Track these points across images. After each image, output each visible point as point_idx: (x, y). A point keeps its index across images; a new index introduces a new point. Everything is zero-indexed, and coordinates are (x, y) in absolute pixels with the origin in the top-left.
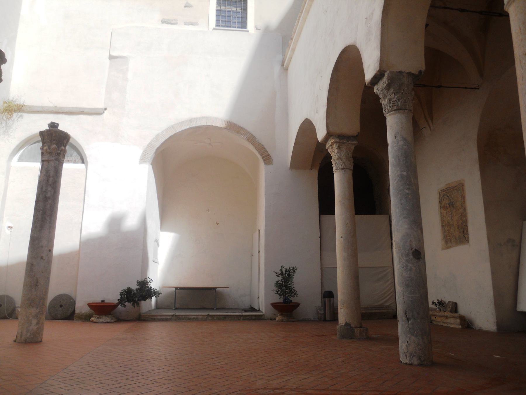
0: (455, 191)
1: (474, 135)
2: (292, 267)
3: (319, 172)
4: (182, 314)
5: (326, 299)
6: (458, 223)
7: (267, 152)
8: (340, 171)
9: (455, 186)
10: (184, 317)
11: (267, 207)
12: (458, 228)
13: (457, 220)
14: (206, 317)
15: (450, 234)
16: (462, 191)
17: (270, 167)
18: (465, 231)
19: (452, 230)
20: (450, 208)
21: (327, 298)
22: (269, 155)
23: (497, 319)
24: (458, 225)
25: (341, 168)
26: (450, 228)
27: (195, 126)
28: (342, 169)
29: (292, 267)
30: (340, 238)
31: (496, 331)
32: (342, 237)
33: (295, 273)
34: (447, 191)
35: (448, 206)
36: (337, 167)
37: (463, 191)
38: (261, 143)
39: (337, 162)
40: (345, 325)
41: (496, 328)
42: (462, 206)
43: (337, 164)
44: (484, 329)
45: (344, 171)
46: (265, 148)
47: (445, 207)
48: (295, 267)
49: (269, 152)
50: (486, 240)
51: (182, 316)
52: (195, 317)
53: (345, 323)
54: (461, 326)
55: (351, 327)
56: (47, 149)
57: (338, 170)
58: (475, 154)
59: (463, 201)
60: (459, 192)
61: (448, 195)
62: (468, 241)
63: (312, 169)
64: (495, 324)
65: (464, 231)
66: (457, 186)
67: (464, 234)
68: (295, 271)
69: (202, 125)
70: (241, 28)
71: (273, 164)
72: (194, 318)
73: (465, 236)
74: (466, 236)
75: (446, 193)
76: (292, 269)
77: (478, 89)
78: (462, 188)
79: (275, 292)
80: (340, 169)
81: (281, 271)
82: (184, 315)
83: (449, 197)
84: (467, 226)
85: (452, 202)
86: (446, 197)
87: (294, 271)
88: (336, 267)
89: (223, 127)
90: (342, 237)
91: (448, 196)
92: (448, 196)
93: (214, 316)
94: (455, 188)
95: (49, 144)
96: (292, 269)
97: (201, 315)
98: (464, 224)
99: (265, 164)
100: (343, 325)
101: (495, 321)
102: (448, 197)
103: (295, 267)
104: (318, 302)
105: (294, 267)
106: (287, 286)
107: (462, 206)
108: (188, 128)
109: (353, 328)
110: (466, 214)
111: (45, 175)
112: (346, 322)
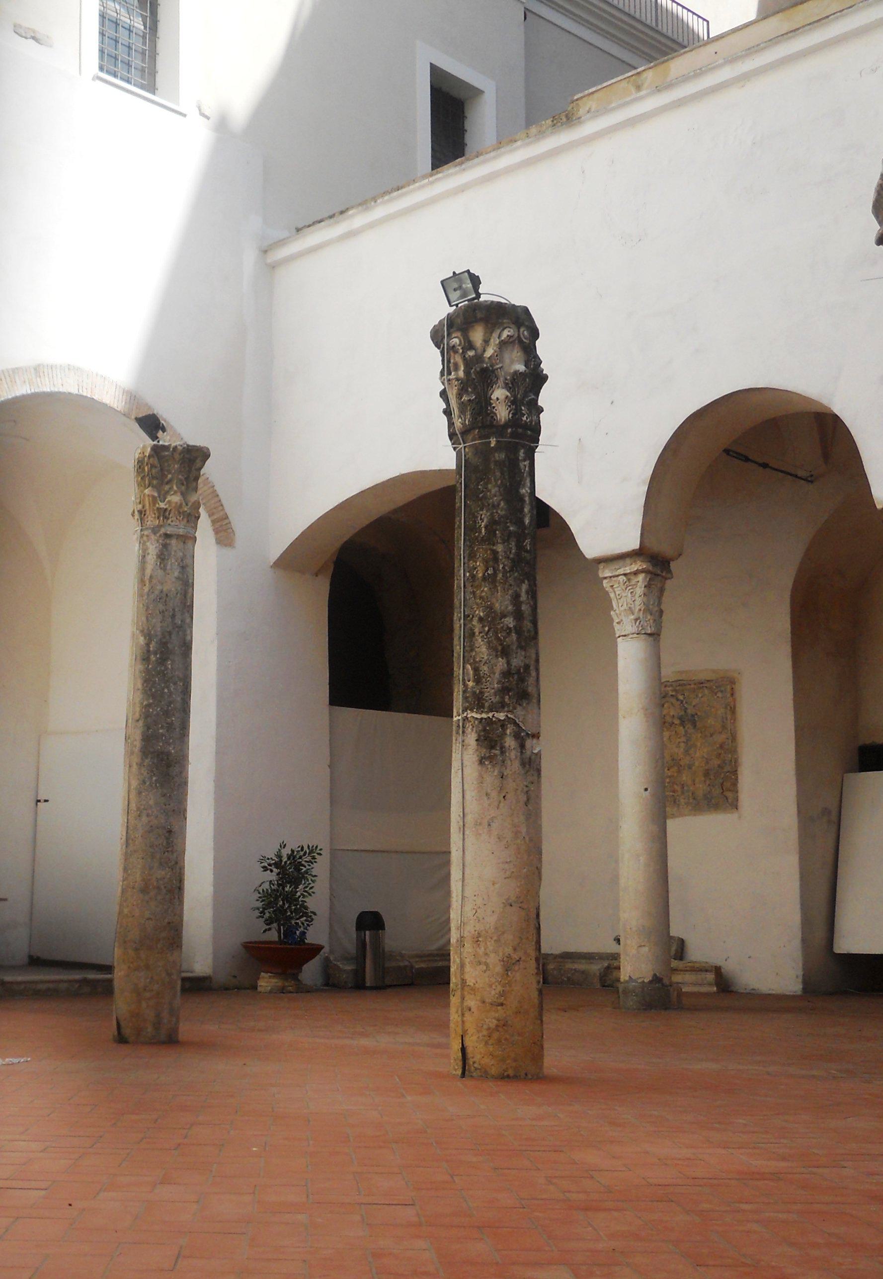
0: (706, 691)
1: (785, 579)
2: (309, 846)
3: (332, 584)
4: (20, 978)
5: (367, 933)
6: (707, 763)
7: (223, 509)
8: (645, 639)
9: (708, 681)
10: (22, 987)
11: (223, 669)
12: (707, 774)
13: (703, 757)
14: (77, 986)
15: (676, 787)
16: (729, 695)
17: (226, 551)
18: (727, 785)
19: (684, 778)
20: (684, 727)
21: (369, 930)
22: (225, 519)
23: (804, 969)
24: (706, 768)
25: (649, 632)
26: (679, 771)
27: (49, 390)
28: (650, 635)
29: (309, 846)
30: (643, 790)
31: (799, 993)
32: (646, 790)
33: (316, 862)
34: (678, 688)
35: (677, 722)
36: (638, 627)
37: (732, 695)
38: (210, 479)
39: (641, 617)
40: (651, 982)
41: (801, 987)
42: (724, 727)
43: (640, 622)
44: (764, 992)
45: (654, 640)
46: (218, 496)
47: (667, 724)
48: (317, 847)
49: (228, 509)
50: (793, 809)
51: (20, 983)
52: (51, 986)
53: (653, 977)
54: (715, 988)
55: (663, 985)
56: (181, 504)
57: (642, 636)
58: (783, 622)
59: (729, 717)
60: (720, 695)
61: (681, 697)
62: (734, 805)
63: (317, 576)
64: (800, 980)
65: (725, 783)
66: (712, 680)
67: (723, 789)
68: (317, 856)
69: (66, 391)
70: (142, 87)
71: (234, 547)
72: (48, 990)
73: (724, 793)
74: (729, 794)
75: (672, 691)
76: (308, 851)
77: (812, 482)
78: (729, 687)
79: (257, 913)
80: (645, 634)
81: (279, 856)
82: (24, 982)
83: (682, 702)
84: (735, 772)
85: (693, 716)
86: (673, 700)
87: (314, 858)
88: (444, 849)
89: (119, 410)
90: (646, 790)
91: (678, 700)
92: (678, 700)
93: (98, 981)
94: (705, 685)
95: (183, 488)
96: (308, 851)
97: (65, 982)
98: (727, 768)
99: (219, 542)
100: (646, 981)
101: (800, 973)
102: (679, 703)
103: (317, 847)
104: (349, 939)
105: (313, 846)
106: (291, 898)
107: (724, 727)
108: (29, 392)
109: (667, 986)
110: (736, 747)
111: (178, 578)
112: (655, 975)
